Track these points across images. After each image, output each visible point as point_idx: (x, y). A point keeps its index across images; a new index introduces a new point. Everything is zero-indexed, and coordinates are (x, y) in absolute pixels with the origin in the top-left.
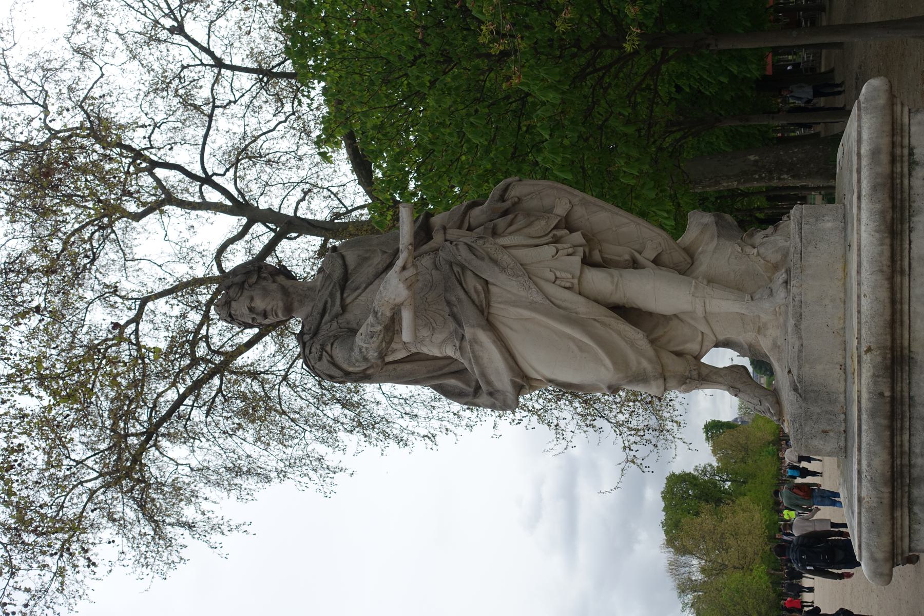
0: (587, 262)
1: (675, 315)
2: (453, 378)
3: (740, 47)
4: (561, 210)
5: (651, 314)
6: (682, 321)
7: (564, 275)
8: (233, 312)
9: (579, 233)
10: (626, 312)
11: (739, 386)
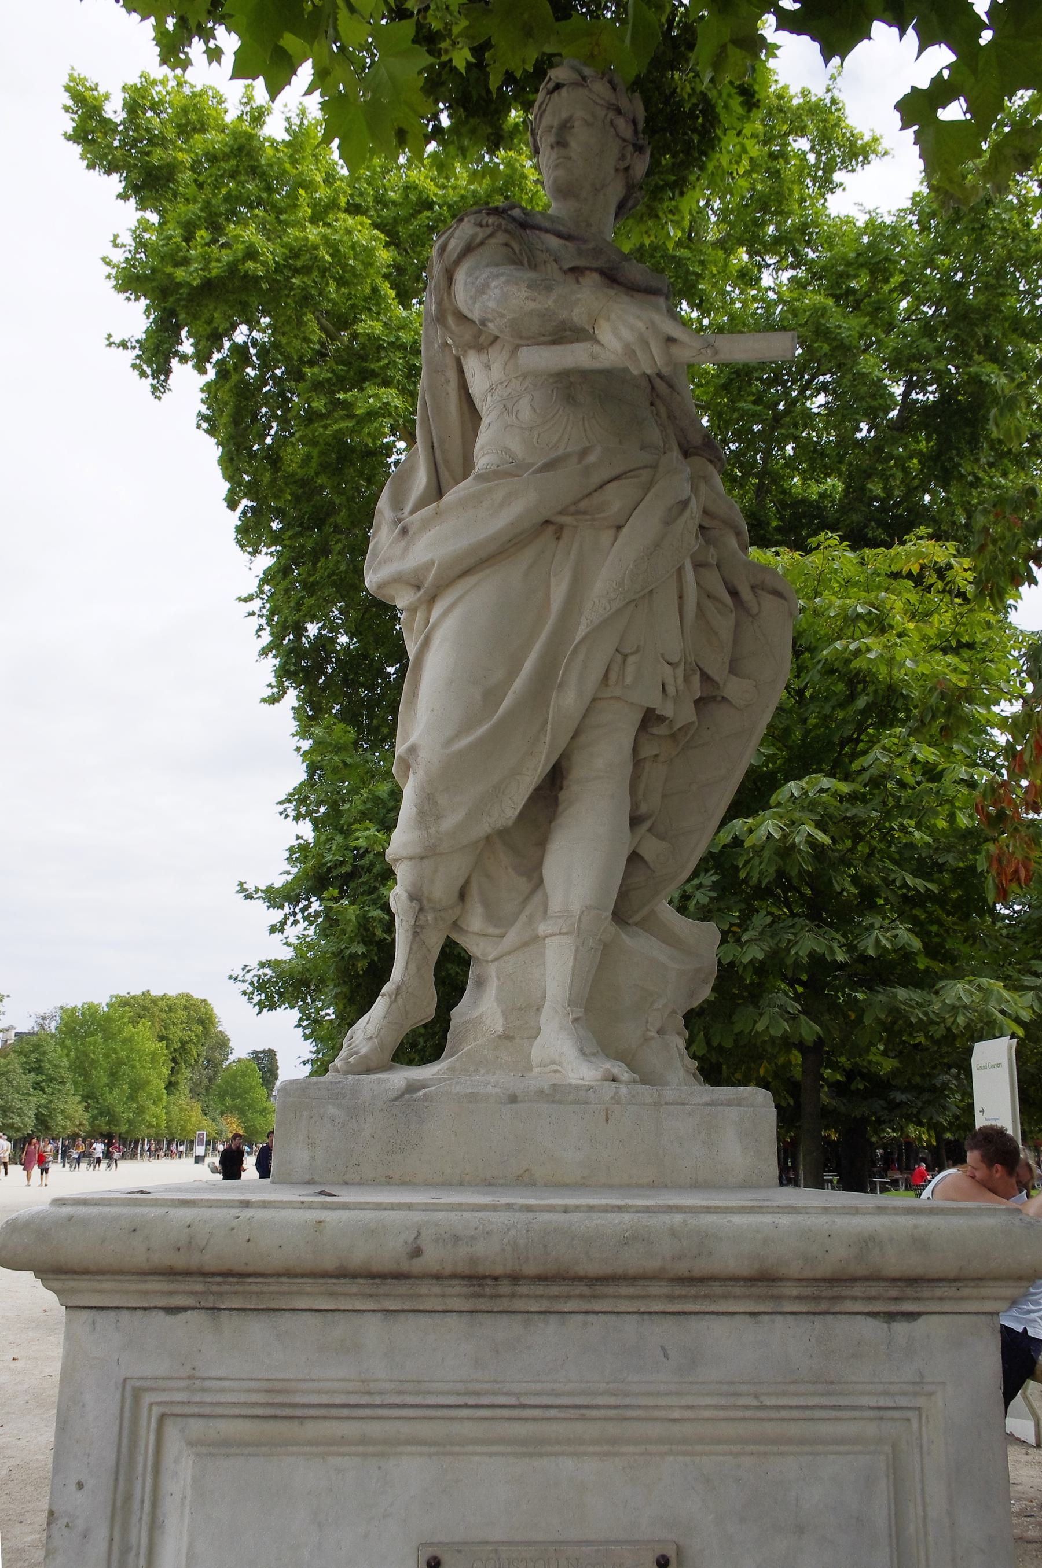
0: (650, 718)
1: (541, 880)
2: (429, 482)
3: (380, 1005)
4: (734, 688)
5: (542, 844)
6: (527, 899)
7: (630, 669)
8: (564, 92)
9: (694, 719)
10: (551, 791)
11: (400, 1001)
